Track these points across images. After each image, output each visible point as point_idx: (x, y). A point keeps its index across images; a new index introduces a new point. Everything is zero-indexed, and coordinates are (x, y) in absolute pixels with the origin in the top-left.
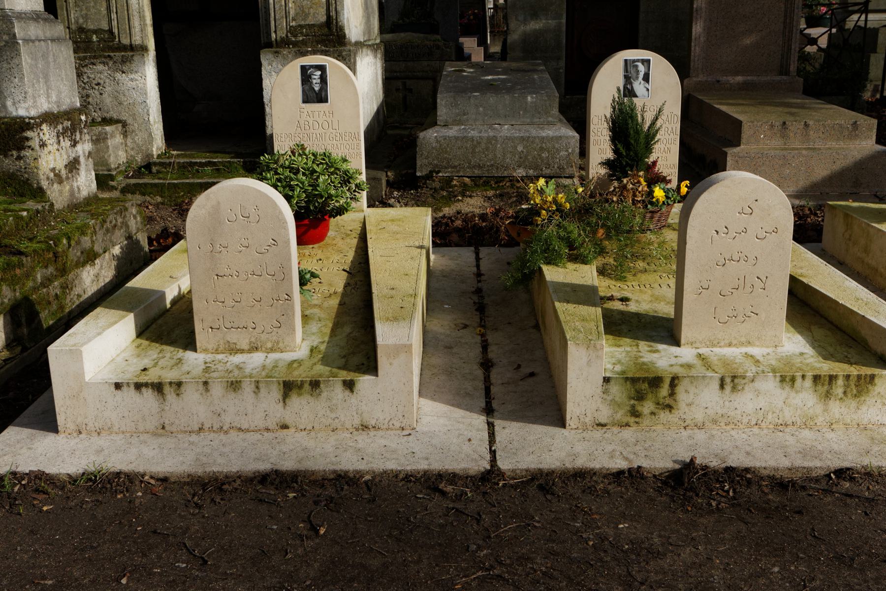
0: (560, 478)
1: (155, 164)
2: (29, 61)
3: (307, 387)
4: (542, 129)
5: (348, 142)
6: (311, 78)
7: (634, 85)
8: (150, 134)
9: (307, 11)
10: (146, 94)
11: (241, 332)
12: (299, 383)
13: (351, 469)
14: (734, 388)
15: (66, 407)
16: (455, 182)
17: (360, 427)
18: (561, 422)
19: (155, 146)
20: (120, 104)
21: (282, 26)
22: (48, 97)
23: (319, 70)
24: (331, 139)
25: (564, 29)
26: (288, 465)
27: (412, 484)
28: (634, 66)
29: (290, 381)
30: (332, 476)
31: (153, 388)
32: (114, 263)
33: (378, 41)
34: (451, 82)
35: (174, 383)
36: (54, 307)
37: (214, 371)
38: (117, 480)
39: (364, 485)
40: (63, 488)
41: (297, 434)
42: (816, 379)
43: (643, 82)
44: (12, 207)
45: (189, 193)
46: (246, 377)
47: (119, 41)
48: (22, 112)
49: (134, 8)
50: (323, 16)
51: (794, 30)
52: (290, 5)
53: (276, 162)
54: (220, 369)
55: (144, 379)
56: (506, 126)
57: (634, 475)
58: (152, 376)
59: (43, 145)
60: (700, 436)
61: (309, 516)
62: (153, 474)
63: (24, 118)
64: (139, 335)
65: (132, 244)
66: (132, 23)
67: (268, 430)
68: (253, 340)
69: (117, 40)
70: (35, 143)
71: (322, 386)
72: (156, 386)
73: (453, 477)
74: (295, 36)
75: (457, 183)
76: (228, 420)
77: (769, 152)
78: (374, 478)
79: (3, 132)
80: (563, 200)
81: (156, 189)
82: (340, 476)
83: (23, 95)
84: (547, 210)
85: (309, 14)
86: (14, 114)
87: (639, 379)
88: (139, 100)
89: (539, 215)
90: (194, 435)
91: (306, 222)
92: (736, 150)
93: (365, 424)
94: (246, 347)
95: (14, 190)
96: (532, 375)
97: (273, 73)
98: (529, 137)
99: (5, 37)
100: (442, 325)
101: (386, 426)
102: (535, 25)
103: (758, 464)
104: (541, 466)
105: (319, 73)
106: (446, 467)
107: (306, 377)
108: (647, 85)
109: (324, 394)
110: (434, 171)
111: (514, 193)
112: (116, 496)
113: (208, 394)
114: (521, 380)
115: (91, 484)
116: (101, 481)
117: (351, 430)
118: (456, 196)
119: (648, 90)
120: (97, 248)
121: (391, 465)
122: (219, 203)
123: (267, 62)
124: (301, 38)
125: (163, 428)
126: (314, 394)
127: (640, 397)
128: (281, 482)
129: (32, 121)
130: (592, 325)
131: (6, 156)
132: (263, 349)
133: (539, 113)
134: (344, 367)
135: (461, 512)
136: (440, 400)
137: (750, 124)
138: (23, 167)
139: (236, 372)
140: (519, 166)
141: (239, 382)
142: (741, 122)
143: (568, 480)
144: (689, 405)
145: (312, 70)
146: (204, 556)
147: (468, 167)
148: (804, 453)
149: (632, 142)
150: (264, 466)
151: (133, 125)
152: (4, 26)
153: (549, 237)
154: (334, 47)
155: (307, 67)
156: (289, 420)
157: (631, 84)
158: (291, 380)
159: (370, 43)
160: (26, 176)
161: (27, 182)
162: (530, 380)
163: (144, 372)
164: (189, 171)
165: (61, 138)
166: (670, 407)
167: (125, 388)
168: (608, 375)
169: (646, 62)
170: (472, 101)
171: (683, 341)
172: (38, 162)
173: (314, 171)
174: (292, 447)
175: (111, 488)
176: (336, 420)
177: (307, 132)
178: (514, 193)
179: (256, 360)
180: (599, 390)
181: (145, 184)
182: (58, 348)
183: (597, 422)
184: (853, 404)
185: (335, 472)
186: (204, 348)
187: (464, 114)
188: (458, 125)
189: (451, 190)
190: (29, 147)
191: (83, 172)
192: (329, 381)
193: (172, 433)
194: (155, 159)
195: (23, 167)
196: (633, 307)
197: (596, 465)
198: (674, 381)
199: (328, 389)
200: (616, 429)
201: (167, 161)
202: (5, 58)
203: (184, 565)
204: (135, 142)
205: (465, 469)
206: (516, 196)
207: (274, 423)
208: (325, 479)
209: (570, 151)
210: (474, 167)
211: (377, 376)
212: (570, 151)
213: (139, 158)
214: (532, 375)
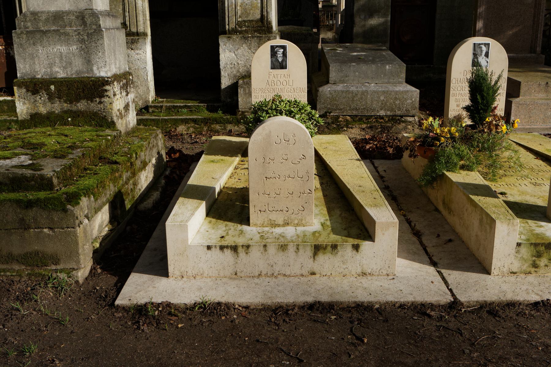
0: (499, 307)
1: (151, 107)
2: (108, 42)
3: (329, 248)
5: (298, 94)
6: (277, 53)
7: (479, 59)
9: (248, 11)
10: (146, 63)
11: (279, 214)
12: (324, 246)
13: (366, 301)
15: (175, 261)
16: (341, 119)
17: (361, 274)
19: (151, 95)
21: (233, 21)
22: (115, 65)
23: (282, 48)
24: (288, 92)
25: (389, 24)
26: (324, 298)
27: (406, 310)
28: (479, 47)
29: (318, 245)
30: (353, 305)
31: (231, 249)
32: (153, 169)
35: (245, 246)
37: (267, 238)
38: (219, 308)
39: (376, 311)
40: (184, 313)
41: (321, 278)
43: (484, 57)
44: (101, 133)
45: (174, 125)
46: (289, 242)
47: (130, 29)
48: (103, 74)
49: (140, 9)
50: (258, 15)
51: (540, 26)
52: (238, 8)
54: (271, 237)
56: (373, 84)
58: (229, 241)
59: (115, 95)
61: (351, 331)
62: (239, 304)
63: (104, 78)
64: (208, 215)
66: (138, 18)
67: (302, 275)
68: (286, 218)
69: (129, 29)
70: (110, 94)
71: (338, 248)
72: (233, 248)
73: (432, 306)
74: (241, 27)
75: (342, 120)
76: (278, 269)
77: (538, 101)
78: (381, 306)
79: (91, 86)
80: (455, 131)
81: (153, 123)
82: (358, 305)
83: (104, 63)
85: (250, 13)
86: (98, 75)
87: (539, 244)
88: (142, 66)
89: (439, 140)
90: (256, 279)
93: (364, 272)
94: (281, 223)
95: (96, 123)
96: (450, 241)
97: (227, 50)
98: (388, 91)
99: (94, 27)
101: (377, 273)
104: (486, 299)
105: (282, 50)
106: (426, 300)
107: (329, 242)
108: (487, 59)
109: (340, 253)
110: (328, 112)
111: (378, 126)
112: (221, 318)
113: (266, 253)
114: (445, 244)
115: (202, 310)
116: (209, 308)
117: (355, 276)
118: (342, 128)
119: (487, 62)
120: (147, 160)
121: (390, 298)
122: (270, 132)
123: (223, 43)
124: (244, 29)
125: (236, 274)
126: (334, 253)
127: (539, 255)
128: (323, 309)
129: (110, 80)
130: (503, 210)
131: (92, 101)
132: (292, 224)
133: (393, 76)
135: (447, 328)
137: (526, 83)
138: (103, 108)
139: (282, 239)
140: (381, 109)
141: (286, 245)
142: (520, 82)
143: (504, 308)
145: (277, 48)
146: (298, 356)
147: (349, 110)
149: (485, 95)
150: (310, 299)
152: (94, 20)
154: (265, 34)
155: (275, 47)
156: (316, 270)
157: (477, 58)
158: (320, 244)
160: (104, 114)
161: (104, 118)
162: (450, 244)
163: (223, 239)
164: (173, 111)
165: (122, 90)
167: (213, 249)
168: (520, 241)
169: (487, 45)
170: (352, 68)
172: (112, 105)
174: (322, 287)
175: (217, 313)
176: (346, 270)
177: (273, 87)
178: (378, 126)
180: (514, 251)
181: (147, 120)
182: (173, 224)
183: (511, 271)
185: (355, 302)
186: (255, 223)
187: (347, 77)
188: (342, 83)
189: (338, 124)
190: (107, 96)
191: (131, 112)
192: (344, 244)
193: (241, 277)
194: (150, 104)
195: (103, 108)
199: (342, 250)
200: (523, 276)
201: (159, 105)
202: (94, 40)
203: (288, 363)
204: (138, 93)
205: (438, 301)
206: (381, 128)
207: (307, 271)
208: (349, 307)
209: (413, 100)
210: (353, 109)
211: (374, 241)
212: (413, 100)
214: (450, 241)
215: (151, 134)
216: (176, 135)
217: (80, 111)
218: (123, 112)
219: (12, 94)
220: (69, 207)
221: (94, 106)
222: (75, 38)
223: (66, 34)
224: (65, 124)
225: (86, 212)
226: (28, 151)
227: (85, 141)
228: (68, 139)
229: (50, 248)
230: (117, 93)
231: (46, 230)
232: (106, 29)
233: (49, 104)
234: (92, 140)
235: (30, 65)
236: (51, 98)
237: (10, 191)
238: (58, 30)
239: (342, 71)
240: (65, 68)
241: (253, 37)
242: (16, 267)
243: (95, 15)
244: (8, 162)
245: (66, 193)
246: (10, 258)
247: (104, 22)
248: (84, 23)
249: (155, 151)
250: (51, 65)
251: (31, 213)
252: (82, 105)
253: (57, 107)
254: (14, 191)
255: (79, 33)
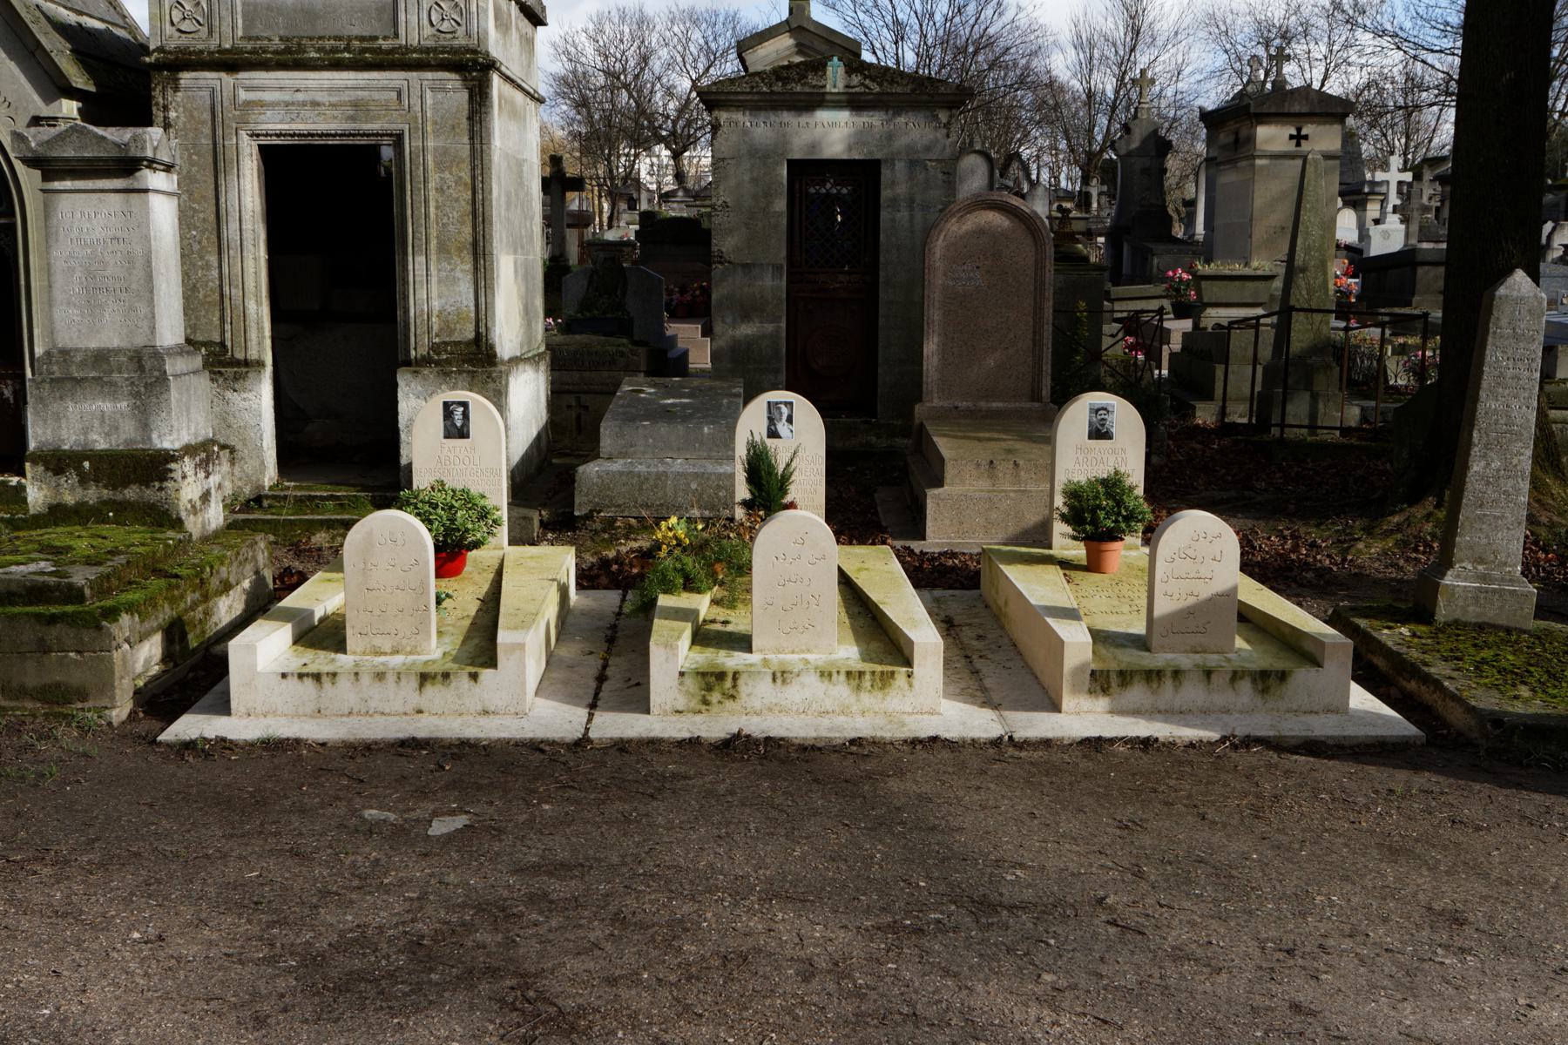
1: (267, 497)
4: (721, 464)
8: (263, 462)
14: (784, 681)
16: (618, 524)
18: (648, 711)
20: (229, 426)
22: (189, 429)
25: (784, 334)
32: (244, 597)
33: (542, 349)
34: (622, 406)
36: (198, 631)
42: (849, 674)
44: (159, 536)
48: (167, 445)
53: (416, 498)
55: (305, 670)
57: (694, 743)
58: (312, 669)
59: (184, 477)
60: (756, 719)
64: (295, 643)
65: (259, 580)
70: (177, 475)
74: (438, 354)
84: (668, 545)
86: (159, 446)
91: (444, 555)
92: (937, 491)
99: (156, 373)
100: (567, 652)
102: (747, 330)
103: (791, 735)
109: (453, 684)
120: (232, 580)
127: (709, 688)
131: (147, 487)
134: (472, 664)
136: (553, 699)
141: (383, 674)
144: (749, 695)
148: (830, 730)
150: (401, 735)
151: (243, 451)
153: (666, 569)
159: (530, 355)
161: (166, 513)
166: (733, 697)
167: (289, 678)
170: (640, 431)
171: (754, 649)
173: (452, 507)
179: (397, 660)
181: (256, 521)
184: (880, 695)
185: (459, 739)
188: (624, 457)
191: (213, 504)
194: (266, 491)
196: (730, 628)
197: (666, 735)
198: (736, 675)
200: (690, 715)
201: (282, 494)
213: (247, 490)
215: (243, 541)
216: (310, 550)
217: (129, 502)
218: (198, 504)
219: (22, 474)
220: (104, 623)
221: (150, 495)
222: (126, 390)
223: (112, 384)
224: (103, 522)
225: (127, 634)
226: (50, 557)
227: (133, 545)
228: (107, 542)
229: (76, 678)
230: (188, 474)
231: (72, 654)
232: (175, 376)
233: (79, 490)
234: (143, 545)
235: (53, 430)
236: (83, 480)
237: (25, 605)
238: (100, 378)
239: (623, 436)
240: (108, 435)
241: (460, 372)
242: (29, 705)
243: (157, 355)
244: (22, 568)
245: (102, 608)
246: (22, 692)
247: (173, 365)
248: (141, 368)
249: (249, 568)
250: (86, 430)
251: (55, 631)
252: (131, 493)
253: (93, 494)
254: (31, 604)
255: (133, 383)
